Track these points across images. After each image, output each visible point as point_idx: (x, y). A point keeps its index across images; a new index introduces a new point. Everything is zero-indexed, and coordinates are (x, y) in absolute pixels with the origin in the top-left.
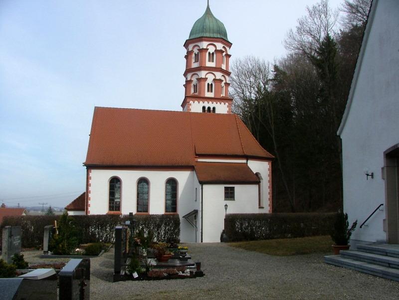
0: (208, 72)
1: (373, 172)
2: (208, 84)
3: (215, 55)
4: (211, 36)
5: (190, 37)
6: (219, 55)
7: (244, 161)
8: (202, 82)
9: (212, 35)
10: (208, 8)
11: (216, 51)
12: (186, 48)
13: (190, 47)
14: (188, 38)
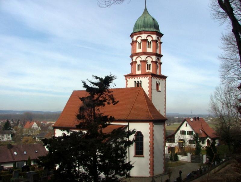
0: (137, 57)
1: (186, 127)
2: (138, 65)
3: (152, 43)
4: (149, 30)
5: (133, 31)
6: (144, 42)
7: (127, 124)
8: (134, 65)
9: (150, 30)
10: (146, 9)
11: (153, 41)
12: (132, 38)
13: (135, 38)
14: (132, 32)
